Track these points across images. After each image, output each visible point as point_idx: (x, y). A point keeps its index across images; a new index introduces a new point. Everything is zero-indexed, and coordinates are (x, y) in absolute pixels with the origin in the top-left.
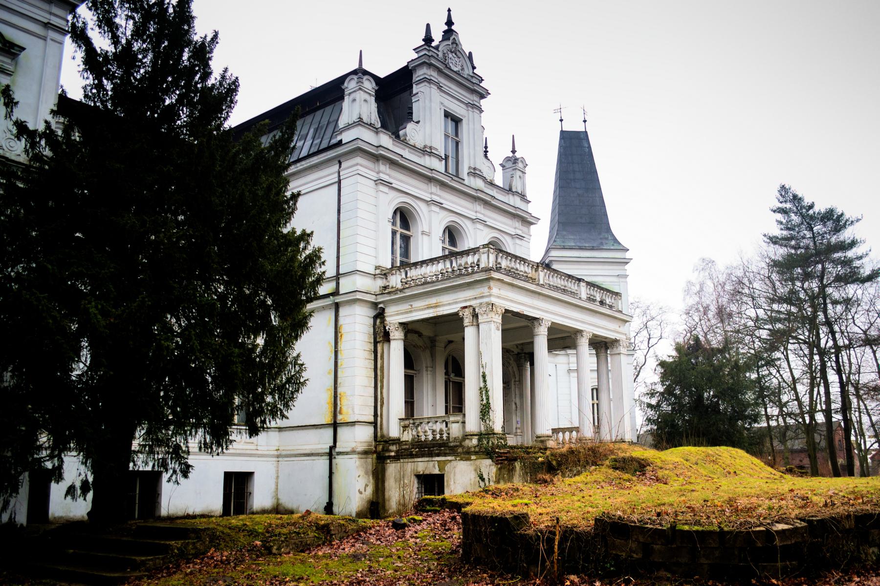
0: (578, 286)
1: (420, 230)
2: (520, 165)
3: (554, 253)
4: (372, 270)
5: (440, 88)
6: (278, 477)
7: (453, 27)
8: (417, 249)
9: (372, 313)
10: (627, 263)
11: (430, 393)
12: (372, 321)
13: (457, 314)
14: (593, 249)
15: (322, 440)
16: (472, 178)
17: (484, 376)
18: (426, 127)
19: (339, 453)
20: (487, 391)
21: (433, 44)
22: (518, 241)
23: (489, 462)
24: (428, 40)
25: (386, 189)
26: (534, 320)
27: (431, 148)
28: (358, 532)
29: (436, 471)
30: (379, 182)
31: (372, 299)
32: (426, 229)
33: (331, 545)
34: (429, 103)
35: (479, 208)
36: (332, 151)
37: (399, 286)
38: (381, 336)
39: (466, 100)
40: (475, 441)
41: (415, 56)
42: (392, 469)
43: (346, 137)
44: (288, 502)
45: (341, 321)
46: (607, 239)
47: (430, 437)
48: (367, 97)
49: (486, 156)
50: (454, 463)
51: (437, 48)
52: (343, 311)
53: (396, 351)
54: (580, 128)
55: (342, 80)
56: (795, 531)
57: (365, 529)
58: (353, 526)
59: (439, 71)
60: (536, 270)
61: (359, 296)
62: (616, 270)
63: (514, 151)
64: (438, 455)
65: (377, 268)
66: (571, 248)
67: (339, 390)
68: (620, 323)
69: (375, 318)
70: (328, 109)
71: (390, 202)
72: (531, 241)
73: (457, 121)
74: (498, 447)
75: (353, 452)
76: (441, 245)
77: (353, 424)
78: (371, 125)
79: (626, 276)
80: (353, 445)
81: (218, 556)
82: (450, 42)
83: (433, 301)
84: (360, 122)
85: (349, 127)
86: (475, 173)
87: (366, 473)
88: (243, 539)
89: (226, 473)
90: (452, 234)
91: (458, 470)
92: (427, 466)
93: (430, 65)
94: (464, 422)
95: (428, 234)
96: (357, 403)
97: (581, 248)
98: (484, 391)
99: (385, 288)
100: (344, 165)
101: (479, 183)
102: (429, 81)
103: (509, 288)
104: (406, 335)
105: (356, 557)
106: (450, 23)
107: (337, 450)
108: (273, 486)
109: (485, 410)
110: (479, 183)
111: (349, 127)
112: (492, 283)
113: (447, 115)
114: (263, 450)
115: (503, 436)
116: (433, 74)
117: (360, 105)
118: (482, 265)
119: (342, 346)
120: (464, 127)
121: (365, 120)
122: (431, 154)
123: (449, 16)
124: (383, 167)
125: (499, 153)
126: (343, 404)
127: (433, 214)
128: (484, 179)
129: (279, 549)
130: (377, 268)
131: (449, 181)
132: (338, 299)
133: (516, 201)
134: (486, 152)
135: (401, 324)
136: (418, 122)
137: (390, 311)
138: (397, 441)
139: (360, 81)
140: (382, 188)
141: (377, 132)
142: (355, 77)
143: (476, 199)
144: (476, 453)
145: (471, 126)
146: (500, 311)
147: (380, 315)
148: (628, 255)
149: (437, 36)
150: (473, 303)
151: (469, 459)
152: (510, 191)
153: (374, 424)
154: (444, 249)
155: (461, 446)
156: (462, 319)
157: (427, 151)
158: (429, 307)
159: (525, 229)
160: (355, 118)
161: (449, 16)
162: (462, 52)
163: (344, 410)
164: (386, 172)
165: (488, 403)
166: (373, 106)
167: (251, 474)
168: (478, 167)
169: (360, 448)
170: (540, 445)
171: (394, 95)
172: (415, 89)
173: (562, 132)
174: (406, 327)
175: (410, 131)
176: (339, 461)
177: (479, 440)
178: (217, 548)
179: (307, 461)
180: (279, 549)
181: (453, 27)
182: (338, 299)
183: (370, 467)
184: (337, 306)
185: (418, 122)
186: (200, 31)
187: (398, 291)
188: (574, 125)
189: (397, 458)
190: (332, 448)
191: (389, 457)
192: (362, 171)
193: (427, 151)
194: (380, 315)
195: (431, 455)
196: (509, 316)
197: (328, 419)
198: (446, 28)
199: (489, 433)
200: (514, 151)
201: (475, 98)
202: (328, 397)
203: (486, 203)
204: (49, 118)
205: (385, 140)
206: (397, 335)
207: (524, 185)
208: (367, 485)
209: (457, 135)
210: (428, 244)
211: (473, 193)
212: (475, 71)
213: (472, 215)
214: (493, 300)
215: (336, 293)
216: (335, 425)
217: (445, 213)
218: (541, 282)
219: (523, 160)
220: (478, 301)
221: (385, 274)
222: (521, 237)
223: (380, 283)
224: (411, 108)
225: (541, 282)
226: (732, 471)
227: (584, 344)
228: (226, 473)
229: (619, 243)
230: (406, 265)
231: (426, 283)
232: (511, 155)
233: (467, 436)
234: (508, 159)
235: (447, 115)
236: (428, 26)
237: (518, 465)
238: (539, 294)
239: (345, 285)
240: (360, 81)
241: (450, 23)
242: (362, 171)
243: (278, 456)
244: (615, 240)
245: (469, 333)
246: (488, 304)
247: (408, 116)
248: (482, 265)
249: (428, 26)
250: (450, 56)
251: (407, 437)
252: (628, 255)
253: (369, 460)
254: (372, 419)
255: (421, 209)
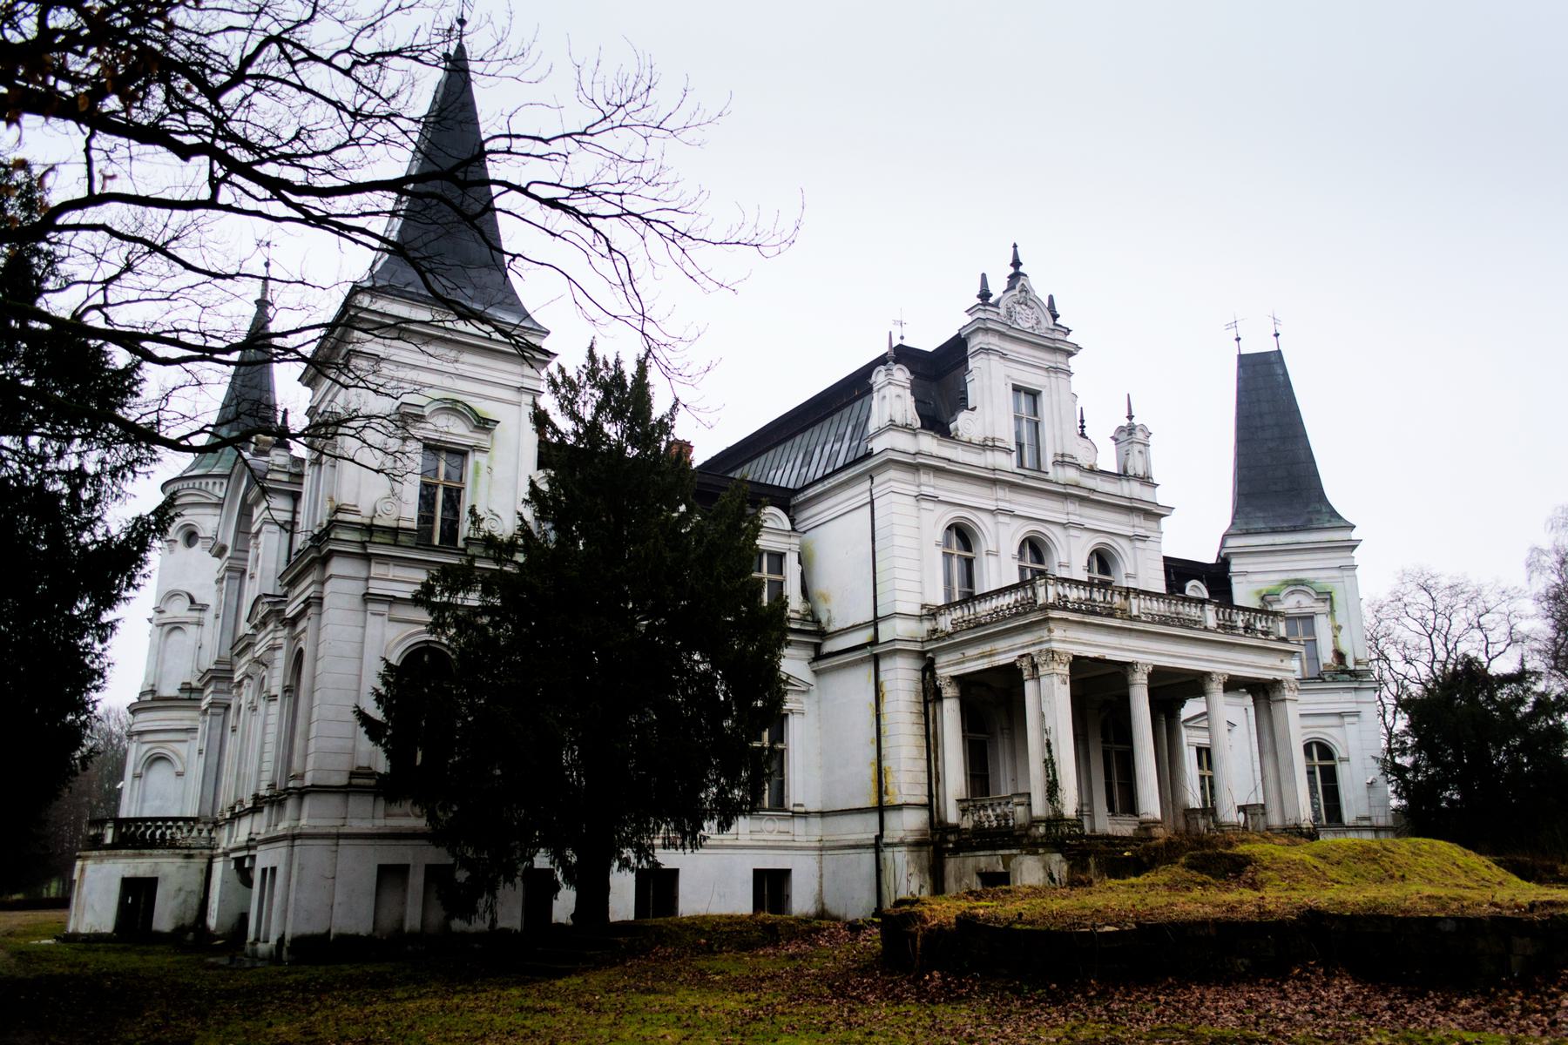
0: (1202, 610)
1: (984, 549)
2: (1140, 436)
3: (1231, 542)
4: (916, 611)
5: (1003, 356)
6: (821, 876)
7: (1021, 269)
8: (981, 575)
9: (919, 664)
10: (1354, 547)
11: (1008, 768)
12: (919, 675)
13: (1013, 664)
14: (1294, 530)
15: (864, 828)
16: (1059, 469)
17: (1049, 745)
18: (988, 409)
19: (888, 845)
20: (1053, 765)
21: (992, 300)
22: (1139, 544)
23: (1058, 857)
24: (985, 295)
25: (930, 505)
26: (1125, 668)
27: (993, 440)
28: (809, 933)
29: (1001, 869)
30: (920, 497)
31: (917, 647)
32: (992, 548)
33: (776, 946)
34: (989, 384)
35: (1072, 507)
36: (862, 464)
37: (950, 629)
38: (930, 695)
39: (1046, 364)
40: (1042, 830)
41: (969, 319)
42: (951, 865)
43: (877, 445)
44: (834, 907)
45: (882, 677)
46: (1319, 512)
47: (995, 824)
48: (899, 391)
49: (1083, 435)
50: (1020, 858)
51: (996, 305)
52: (883, 665)
53: (950, 713)
54: (1266, 345)
55: (866, 373)
56: (1120, 934)
57: (818, 930)
58: (805, 927)
59: (1002, 334)
60: (1127, 598)
61: (898, 646)
62: (1337, 559)
63: (1130, 417)
64: (1002, 848)
65: (923, 606)
66: (1258, 533)
67: (885, 764)
68: (1281, 656)
69: (924, 671)
70: (858, 404)
71: (937, 520)
72: (1163, 541)
73: (1034, 395)
74: (1069, 837)
75: (901, 843)
76: (1015, 565)
77: (899, 807)
78: (906, 426)
79: (1354, 567)
80: (902, 834)
81: (662, 952)
82: (1016, 292)
83: (987, 648)
84: (893, 425)
85: (880, 432)
86: (1062, 461)
87: (921, 871)
88: (688, 937)
89: (756, 872)
90: (1034, 547)
91: (1024, 867)
92: (988, 861)
93: (987, 330)
94: (1030, 805)
95: (996, 554)
96: (907, 782)
97: (1274, 531)
98: (1050, 764)
99: (935, 631)
100: (876, 480)
101: (1071, 474)
102: (987, 351)
103: (1081, 628)
104: (962, 692)
105: (792, 957)
106: (1016, 263)
107: (885, 840)
108: (817, 887)
109: (1052, 788)
110: (1071, 474)
111: (880, 432)
112: (1052, 625)
113: (1017, 389)
114: (801, 840)
115: (1078, 822)
116: (993, 341)
117: (894, 399)
118: (1040, 602)
119: (885, 708)
120: (1044, 400)
121: (899, 421)
122: (994, 448)
123: (1016, 254)
124: (924, 478)
125: (1102, 430)
126: (890, 781)
127: (1001, 527)
128: (1079, 467)
129: (720, 947)
130: (923, 606)
131: (1029, 478)
132: (877, 650)
133: (1134, 489)
134: (1082, 427)
135: (953, 678)
136: (973, 409)
137: (941, 660)
138: (955, 828)
139: (889, 372)
140: (924, 504)
141: (914, 432)
142: (882, 368)
143: (1066, 497)
144: (1043, 845)
145: (1055, 397)
146: (1065, 659)
147: (928, 668)
148: (1354, 535)
149: (997, 288)
150: (1031, 650)
151: (1036, 853)
152: (1123, 475)
153: (929, 806)
154: (1022, 570)
155: (1027, 835)
156: (1020, 671)
157: (987, 446)
158: (983, 656)
159: (1151, 524)
160: (885, 421)
161: (1016, 254)
162: (1037, 302)
163: (890, 788)
164: (930, 484)
165: (1055, 780)
166: (909, 401)
167: (788, 872)
168: (1067, 452)
169: (910, 839)
170: (1143, 834)
171: (939, 377)
172: (972, 363)
173: (1240, 357)
174: (958, 680)
175: (963, 423)
176: (888, 854)
177: (1048, 828)
178: (663, 946)
179: (852, 855)
180: (720, 947)
181: (1021, 269)
182: (877, 650)
183: (925, 863)
184: (876, 659)
185: (973, 409)
186: (659, 410)
187: (949, 635)
188: (1257, 344)
189: (955, 852)
190: (879, 837)
191: (948, 850)
192: (897, 486)
193: (987, 446)
194: (928, 668)
195: (993, 847)
196: (1078, 663)
197: (871, 801)
198: (1012, 270)
199: (1056, 820)
200: (1130, 417)
201: (1059, 359)
202: (871, 772)
203: (1083, 500)
204: (521, 508)
205: (929, 443)
206: (949, 691)
207: (1147, 463)
208: (921, 887)
209: (1036, 414)
210: (998, 568)
211: (1061, 490)
212: (1059, 321)
213: (1063, 519)
214: (1055, 646)
215: (875, 642)
216: (881, 809)
217: (1020, 521)
218: (1135, 612)
219: (1143, 429)
220: (1037, 648)
221: (932, 613)
222: (1144, 538)
223: (927, 625)
224: (965, 392)
225: (1135, 612)
226: (1398, 874)
227: (1216, 688)
228: (756, 872)
229: (1340, 517)
230: (970, 598)
231: (979, 625)
232: (1125, 422)
233: (1034, 822)
234: (1121, 429)
235: (1017, 389)
236: (984, 276)
237: (1092, 861)
238: (1130, 630)
239: (886, 632)
240: (889, 372)
241: (1016, 263)
242: (897, 486)
243: (821, 849)
244: (1334, 514)
245: (1030, 687)
246: (1048, 651)
247: (961, 402)
248: (1040, 602)
249: (984, 276)
250: (1018, 308)
251: (967, 823)
252: (1354, 535)
253: (924, 854)
254: (925, 800)
255: (984, 523)
